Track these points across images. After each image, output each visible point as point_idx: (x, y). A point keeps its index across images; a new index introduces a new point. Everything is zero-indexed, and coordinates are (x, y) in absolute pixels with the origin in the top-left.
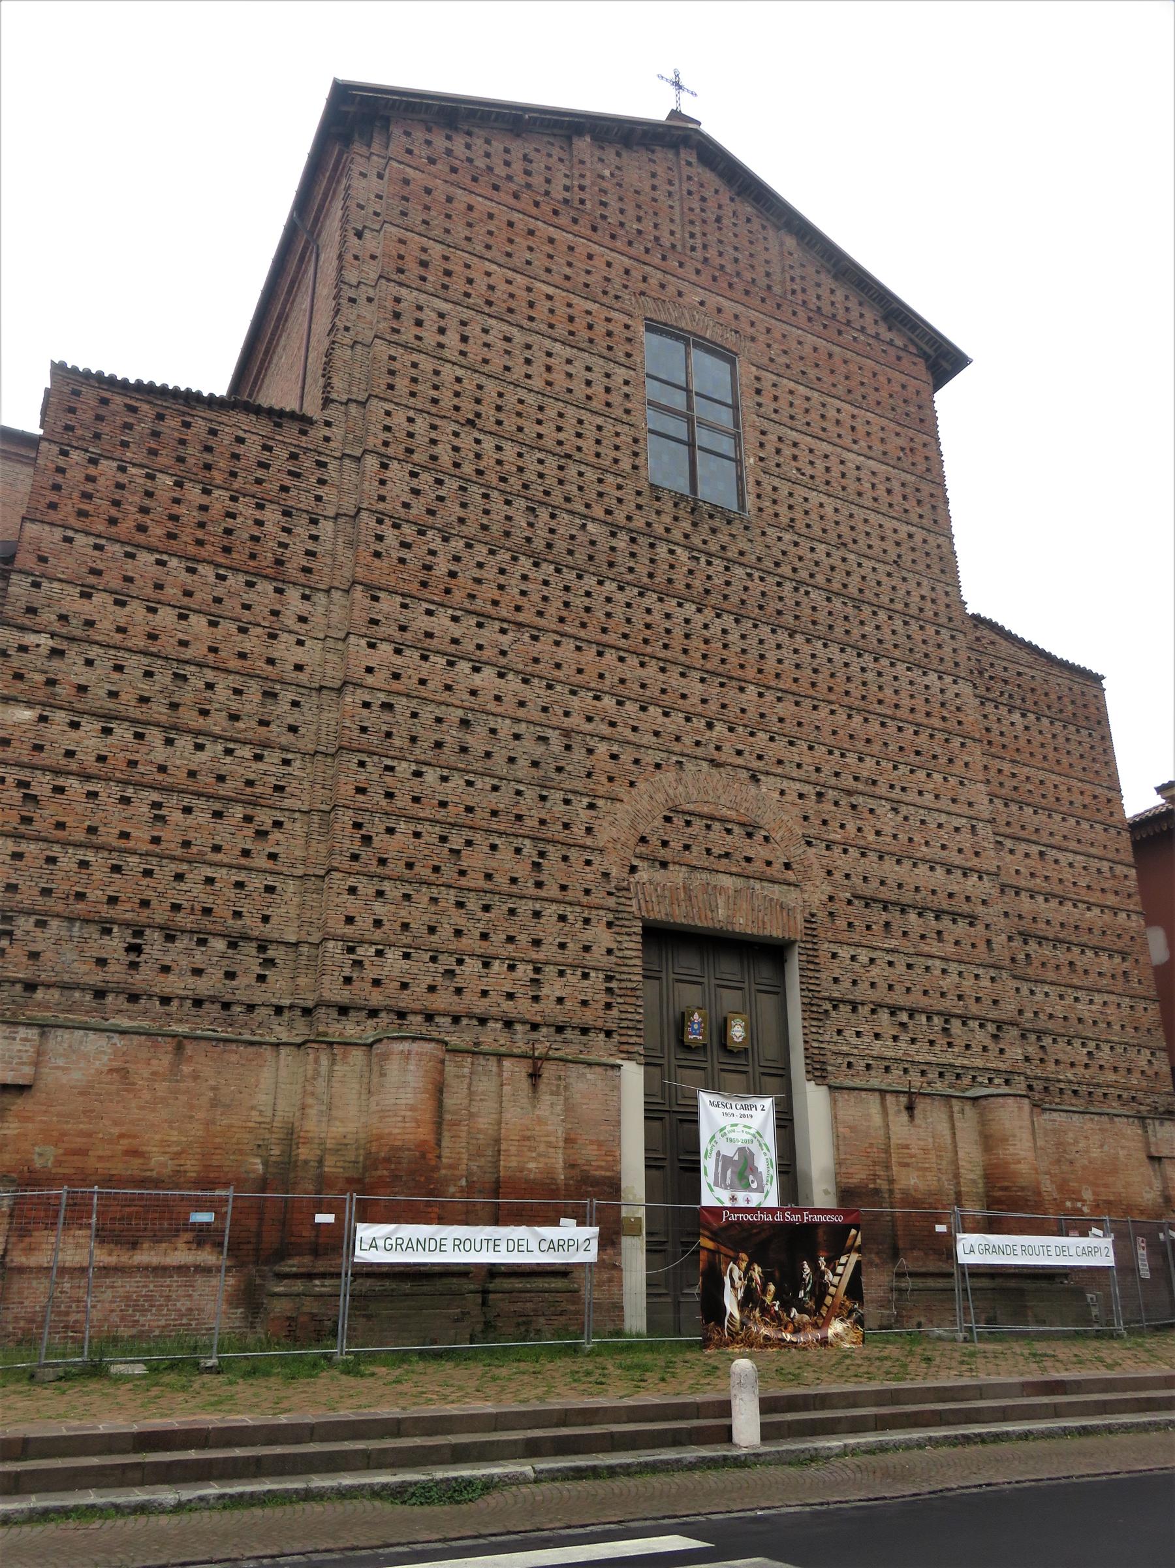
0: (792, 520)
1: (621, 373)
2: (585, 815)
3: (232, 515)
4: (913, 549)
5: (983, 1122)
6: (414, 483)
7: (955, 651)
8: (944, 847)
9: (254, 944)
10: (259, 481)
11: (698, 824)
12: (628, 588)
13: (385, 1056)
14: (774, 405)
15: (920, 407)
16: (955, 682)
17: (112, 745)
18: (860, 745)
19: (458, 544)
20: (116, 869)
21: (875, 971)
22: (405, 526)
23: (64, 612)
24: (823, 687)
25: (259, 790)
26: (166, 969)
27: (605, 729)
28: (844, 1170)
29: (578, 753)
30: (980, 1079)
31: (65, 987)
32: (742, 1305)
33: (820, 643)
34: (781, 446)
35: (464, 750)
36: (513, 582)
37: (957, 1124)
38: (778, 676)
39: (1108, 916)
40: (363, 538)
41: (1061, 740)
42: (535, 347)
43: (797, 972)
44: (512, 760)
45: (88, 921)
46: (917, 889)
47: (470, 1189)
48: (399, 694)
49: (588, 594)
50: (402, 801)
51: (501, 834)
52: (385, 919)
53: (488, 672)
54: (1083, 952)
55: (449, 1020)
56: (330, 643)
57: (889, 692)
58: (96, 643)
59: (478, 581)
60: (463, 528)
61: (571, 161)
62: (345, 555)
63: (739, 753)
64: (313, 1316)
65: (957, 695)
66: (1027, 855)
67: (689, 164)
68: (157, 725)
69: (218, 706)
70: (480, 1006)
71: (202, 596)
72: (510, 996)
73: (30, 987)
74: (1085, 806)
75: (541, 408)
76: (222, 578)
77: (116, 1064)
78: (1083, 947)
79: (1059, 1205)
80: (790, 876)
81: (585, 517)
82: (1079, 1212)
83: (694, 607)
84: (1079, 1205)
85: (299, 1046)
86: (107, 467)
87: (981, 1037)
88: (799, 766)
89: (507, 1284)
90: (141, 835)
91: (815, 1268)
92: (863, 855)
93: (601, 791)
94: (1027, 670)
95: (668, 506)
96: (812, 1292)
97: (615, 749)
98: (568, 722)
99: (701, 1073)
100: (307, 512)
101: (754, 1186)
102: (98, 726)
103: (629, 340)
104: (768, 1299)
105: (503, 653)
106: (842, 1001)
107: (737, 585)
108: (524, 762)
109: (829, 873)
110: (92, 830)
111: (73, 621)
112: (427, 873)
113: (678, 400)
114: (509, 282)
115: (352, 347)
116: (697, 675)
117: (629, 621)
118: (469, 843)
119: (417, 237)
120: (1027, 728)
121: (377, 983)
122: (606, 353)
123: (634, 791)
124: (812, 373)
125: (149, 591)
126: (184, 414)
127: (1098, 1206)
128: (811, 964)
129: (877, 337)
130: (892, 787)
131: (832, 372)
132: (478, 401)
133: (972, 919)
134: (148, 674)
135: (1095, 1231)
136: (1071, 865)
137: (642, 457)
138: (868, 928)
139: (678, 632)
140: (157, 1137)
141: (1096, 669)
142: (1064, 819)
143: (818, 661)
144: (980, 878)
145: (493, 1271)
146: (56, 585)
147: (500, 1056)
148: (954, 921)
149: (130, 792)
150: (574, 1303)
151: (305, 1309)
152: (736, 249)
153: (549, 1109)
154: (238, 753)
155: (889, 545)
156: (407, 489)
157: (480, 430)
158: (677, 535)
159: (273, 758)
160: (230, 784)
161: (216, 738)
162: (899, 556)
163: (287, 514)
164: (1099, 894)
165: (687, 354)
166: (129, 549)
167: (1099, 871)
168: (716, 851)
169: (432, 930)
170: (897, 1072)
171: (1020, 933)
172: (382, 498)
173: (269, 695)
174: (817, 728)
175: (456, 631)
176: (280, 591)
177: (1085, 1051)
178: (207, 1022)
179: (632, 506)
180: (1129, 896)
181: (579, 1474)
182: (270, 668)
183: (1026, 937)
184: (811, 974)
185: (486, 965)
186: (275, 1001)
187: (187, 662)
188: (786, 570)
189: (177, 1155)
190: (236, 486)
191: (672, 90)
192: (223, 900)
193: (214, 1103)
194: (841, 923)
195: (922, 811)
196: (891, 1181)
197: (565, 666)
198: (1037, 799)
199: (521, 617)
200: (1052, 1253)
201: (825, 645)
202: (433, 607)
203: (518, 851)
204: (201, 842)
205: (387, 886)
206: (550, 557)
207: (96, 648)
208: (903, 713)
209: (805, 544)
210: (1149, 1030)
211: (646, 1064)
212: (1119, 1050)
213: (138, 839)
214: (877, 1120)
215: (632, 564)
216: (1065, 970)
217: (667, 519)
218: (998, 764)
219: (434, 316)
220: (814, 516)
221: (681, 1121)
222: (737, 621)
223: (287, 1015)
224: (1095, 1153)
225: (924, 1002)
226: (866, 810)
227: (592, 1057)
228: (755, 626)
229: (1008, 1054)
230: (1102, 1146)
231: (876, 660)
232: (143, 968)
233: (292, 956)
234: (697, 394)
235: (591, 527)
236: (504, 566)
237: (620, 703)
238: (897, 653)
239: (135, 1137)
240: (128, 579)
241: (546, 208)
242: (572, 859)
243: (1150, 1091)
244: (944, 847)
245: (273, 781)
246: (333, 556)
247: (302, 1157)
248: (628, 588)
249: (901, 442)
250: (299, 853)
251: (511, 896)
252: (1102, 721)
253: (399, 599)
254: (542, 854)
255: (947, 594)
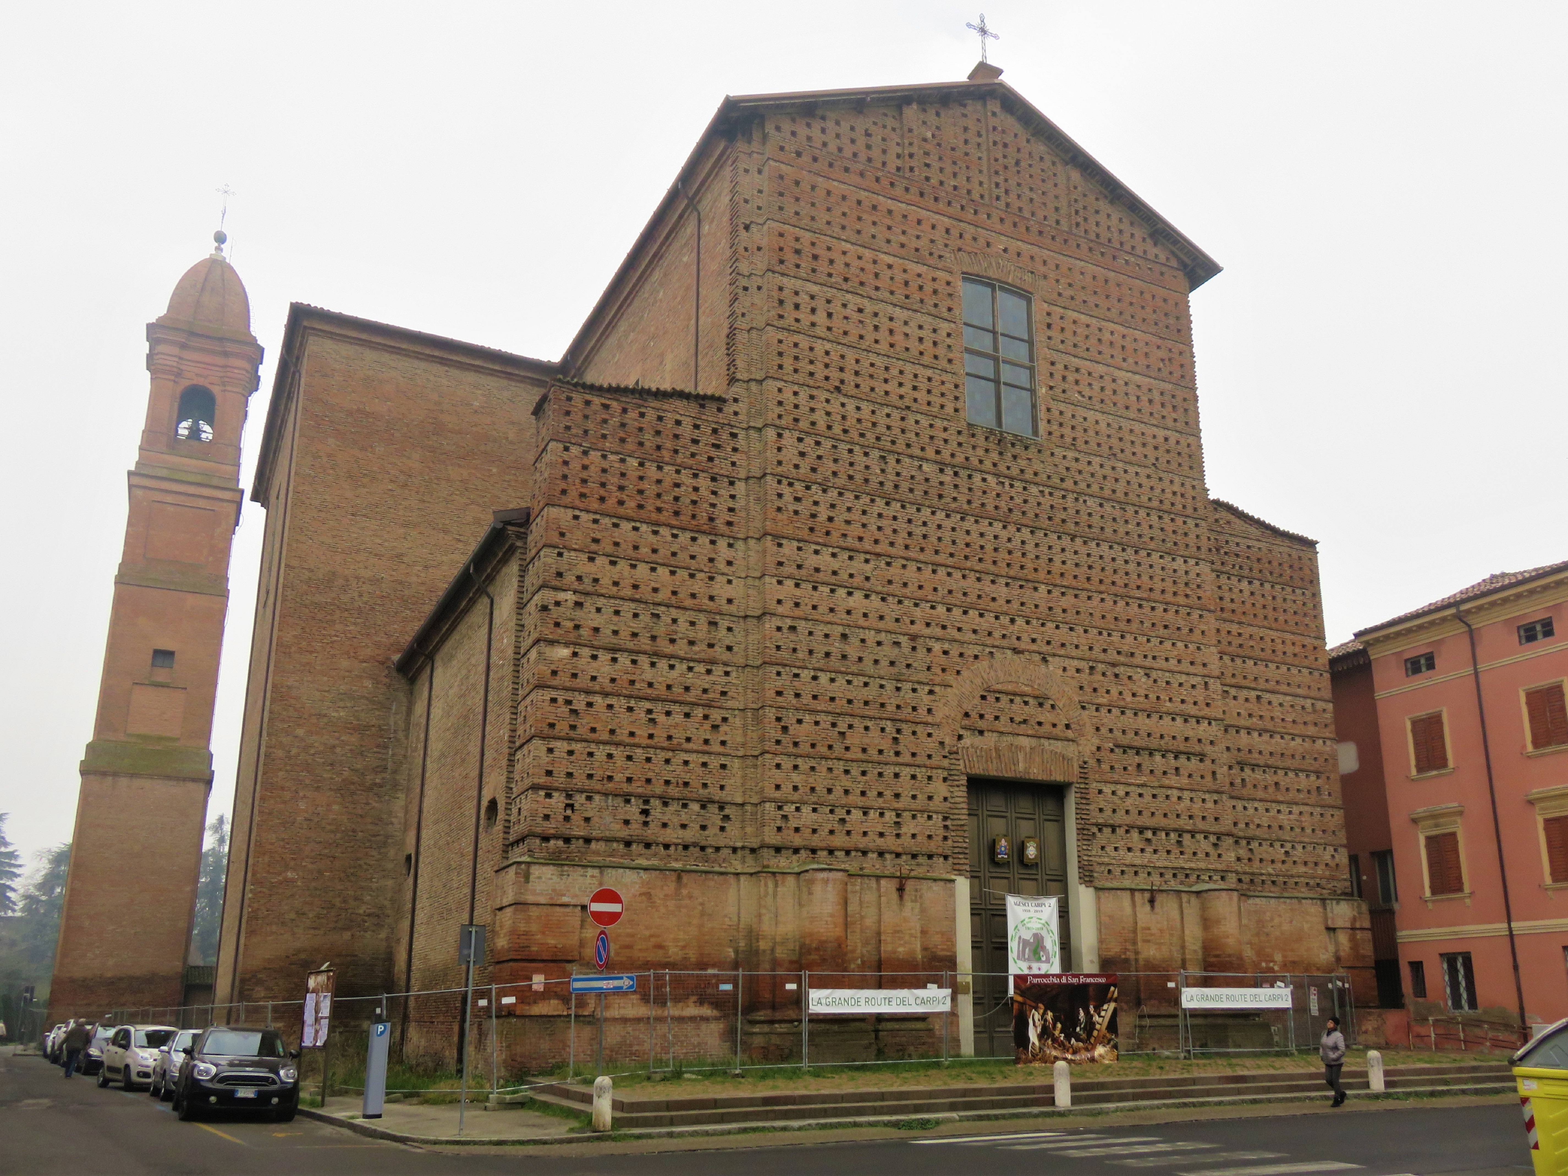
0: (1074, 439)
1: (945, 327)
2: (926, 699)
3: (677, 485)
4: (1168, 451)
5: (1204, 908)
6: (801, 447)
7: (1198, 536)
8: (1183, 701)
9: (716, 805)
10: (693, 455)
11: (1005, 699)
12: (953, 515)
13: (812, 882)
14: (1061, 337)
15: (1178, 318)
16: (1197, 564)
17: (619, 670)
18: (1122, 625)
19: (833, 494)
20: (629, 758)
21: (1129, 801)
22: (796, 483)
23: (579, 573)
24: (1095, 580)
25: (711, 695)
26: (665, 825)
27: (938, 632)
28: (1104, 946)
29: (921, 652)
30: (1203, 877)
31: (608, 840)
32: (1040, 1037)
33: (1094, 543)
34: (1067, 373)
35: (844, 657)
36: (872, 520)
37: (1185, 911)
38: (1062, 575)
39: (1307, 744)
40: (769, 498)
41: (1279, 600)
42: (881, 314)
43: (1074, 806)
44: (876, 662)
45: (616, 795)
46: (1162, 736)
47: (863, 966)
48: (800, 618)
49: (925, 524)
50: (806, 699)
51: (871, 718)
52: (800, 785)
53: (858, 595)
54: (1286, 774)
55: (843, 853)
56: (750, 581)
57: (1145, 578)
58: (603, 595)
59: (848, 522)
60: (836, 480)
61: (901, 129)
62: (755, 509)
63: (1034, 641)
64: (777, 1046)
65: (1198, 575)
66: (1247, 700)
67: (994, 114)
68: (645, 653)
69: (681, 635)
70: (863, 843)
71: (664, 552)
72: (881, 835)
73: (588, 841)
74: (1295, 655)
75: (887, 369)
76: (675, 536)
77: (644, 890)
78: (1286, 770)
79: (1256, 966)
80: (1070, 734)
81: (922, 459)
82: (1271, 970)
83: (1001, 525)
84: (1271, 965)
85: (751, 874)
86: (595, 455)
87: (1205, 845)
88: (1077, 647)
89: (889, 1025)
90: (642, 733)
91: (1087, 1013)
92: (1123, 713)
93: (938, 680)
94: (1255, 543)
95: (980, 441)
96: (1085, 1029)
97: (946, 646)
98: (914, 629)
99: (1006, 881)
100: (727, 477)
101: (1044, 959)
102: (609, 656)
103: (950, 295)
104: (1057, 1033)
105: (867, 579)
106: (1106, 826)
107: (1032, 501)
108: (884, 663)
109: (1098, 729)
110: (612, 732)
111: (586, 580)
112: (824, 750)
113: (985, 342)
114: (860, 258)
115: (749, 331)
116: (1003, 581)
117: (954, 542)
118: (850, 727)
119: (791, 228)
120: (1252, 593)
121: (797, 830)
122: (933, 310)
123: (960, 678)
124: (1092, 300)
125: (630, 552)
126: (640, 406)
127: (1285, 965)
128: (1084, 796)
129: (1144, 256)
130: (1145, 657)
131: (1107, 297)
132: (842, 369)
133: (1202, 757)
134: (636, 615)
135: (1279, 983)
136: (1281, 705)
137: (961, 400)
138: (1125, 769)
139: (989, 547)
140: (672, 936)
141: (1311, 537)
142: (1278, 667)
143: (1092, 559)
144: (1210, 724)
145: (880, 1018)
146: (573, 553)
147: (878, 878)
148: (1188, 759)
149: (632, 703)
150: (931, 1037)
151: (773, 1041)
152: (1031, 189)
153: (910, 910)
154: (696, 669)
155: (1149, 451)
156: (796, 452)
157: (846, 395)
158: (988, 465)
159: (718, 670)
160: (693, 692)
161: (682, 659)
162: (1157, 459)
163: (713, 479)
164: (1302, 726)
165: (994, 298)
166: (615, 520)
167: (1303, 708)
168: (1018, 719)
169: (830, 791)
170: (1143, 875)
171: (1238, 763)
172: (780, 463)
173: (713, 624)
174: (1091, 614)
175: (835, 564)
176: (713, 542)
177: (1283, 850)
178: (691, 861)
179: (955, 444)
180: (1326, 726)
181: (980, 1118)
182: (711, 603)
183: (1242, 765)
184: (1083, 807)
185: (865, 814)
186: (731, 844)
187: (659, 604)
188: (1069, 484)
189: (683, 948)
190: (679, 461)
191: (976, 35)
192: (695, 775)
193: (703, 914)
194: (1105, 767)
195: (1167, 674)
196: (1137, 953)
197: (910, 584)
198: (1257, 653)
199: (878, 549)
200: (1248, 999)
201: (1098, 545)
202: (818, 548)
203: (883, 730)
204: (679, 736)
205: (799, 762)
206: (897, 497)
207: (602, 599)
208: (1156, 595)
209: (1084, 459)
210: (1334, 832)
211: (972, 877)
212: (1309, 848)
213: (640, 736)
214: (1128, 910)
215: (955, 495)
216: (1271, 789)
217: (980, 452)
218: (1227, 626)
219: (807, 298)
220: (1091, 433)
221: (993, 915)
222: (1032, 532)
223: (739, 852)
224: (1286, 927)
225: (1164, 822)
226: (1125, 678)
227: (935, 875)
228: (1046, 535)
229: (1224, 857)
230: (1291, 922)
231: (1136, 552)
232: (652, 825)
233: (740, 812)
234: (1002, 335)
235: (926, 467)
236: (865, 508)
237: (949, 610)
238: (1152, 545)
239: (658, 936)
240: (617, 544)
241: (885, 182)
242: (919, 733)
243: (1332, 878)
244: (1183, 701)
245: (720, 688)
246: (747, 511)
247: (762, 948)
248: (953, 515)
249: (1162, 354)
250: (740, 739)
251: (879, 763)
252: (1313, 580)
253: (795, 544)
254: (899, 731)
255: (1194, 487)
